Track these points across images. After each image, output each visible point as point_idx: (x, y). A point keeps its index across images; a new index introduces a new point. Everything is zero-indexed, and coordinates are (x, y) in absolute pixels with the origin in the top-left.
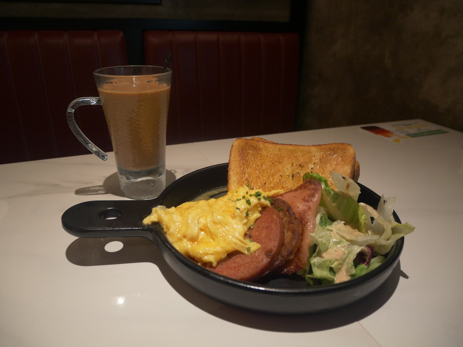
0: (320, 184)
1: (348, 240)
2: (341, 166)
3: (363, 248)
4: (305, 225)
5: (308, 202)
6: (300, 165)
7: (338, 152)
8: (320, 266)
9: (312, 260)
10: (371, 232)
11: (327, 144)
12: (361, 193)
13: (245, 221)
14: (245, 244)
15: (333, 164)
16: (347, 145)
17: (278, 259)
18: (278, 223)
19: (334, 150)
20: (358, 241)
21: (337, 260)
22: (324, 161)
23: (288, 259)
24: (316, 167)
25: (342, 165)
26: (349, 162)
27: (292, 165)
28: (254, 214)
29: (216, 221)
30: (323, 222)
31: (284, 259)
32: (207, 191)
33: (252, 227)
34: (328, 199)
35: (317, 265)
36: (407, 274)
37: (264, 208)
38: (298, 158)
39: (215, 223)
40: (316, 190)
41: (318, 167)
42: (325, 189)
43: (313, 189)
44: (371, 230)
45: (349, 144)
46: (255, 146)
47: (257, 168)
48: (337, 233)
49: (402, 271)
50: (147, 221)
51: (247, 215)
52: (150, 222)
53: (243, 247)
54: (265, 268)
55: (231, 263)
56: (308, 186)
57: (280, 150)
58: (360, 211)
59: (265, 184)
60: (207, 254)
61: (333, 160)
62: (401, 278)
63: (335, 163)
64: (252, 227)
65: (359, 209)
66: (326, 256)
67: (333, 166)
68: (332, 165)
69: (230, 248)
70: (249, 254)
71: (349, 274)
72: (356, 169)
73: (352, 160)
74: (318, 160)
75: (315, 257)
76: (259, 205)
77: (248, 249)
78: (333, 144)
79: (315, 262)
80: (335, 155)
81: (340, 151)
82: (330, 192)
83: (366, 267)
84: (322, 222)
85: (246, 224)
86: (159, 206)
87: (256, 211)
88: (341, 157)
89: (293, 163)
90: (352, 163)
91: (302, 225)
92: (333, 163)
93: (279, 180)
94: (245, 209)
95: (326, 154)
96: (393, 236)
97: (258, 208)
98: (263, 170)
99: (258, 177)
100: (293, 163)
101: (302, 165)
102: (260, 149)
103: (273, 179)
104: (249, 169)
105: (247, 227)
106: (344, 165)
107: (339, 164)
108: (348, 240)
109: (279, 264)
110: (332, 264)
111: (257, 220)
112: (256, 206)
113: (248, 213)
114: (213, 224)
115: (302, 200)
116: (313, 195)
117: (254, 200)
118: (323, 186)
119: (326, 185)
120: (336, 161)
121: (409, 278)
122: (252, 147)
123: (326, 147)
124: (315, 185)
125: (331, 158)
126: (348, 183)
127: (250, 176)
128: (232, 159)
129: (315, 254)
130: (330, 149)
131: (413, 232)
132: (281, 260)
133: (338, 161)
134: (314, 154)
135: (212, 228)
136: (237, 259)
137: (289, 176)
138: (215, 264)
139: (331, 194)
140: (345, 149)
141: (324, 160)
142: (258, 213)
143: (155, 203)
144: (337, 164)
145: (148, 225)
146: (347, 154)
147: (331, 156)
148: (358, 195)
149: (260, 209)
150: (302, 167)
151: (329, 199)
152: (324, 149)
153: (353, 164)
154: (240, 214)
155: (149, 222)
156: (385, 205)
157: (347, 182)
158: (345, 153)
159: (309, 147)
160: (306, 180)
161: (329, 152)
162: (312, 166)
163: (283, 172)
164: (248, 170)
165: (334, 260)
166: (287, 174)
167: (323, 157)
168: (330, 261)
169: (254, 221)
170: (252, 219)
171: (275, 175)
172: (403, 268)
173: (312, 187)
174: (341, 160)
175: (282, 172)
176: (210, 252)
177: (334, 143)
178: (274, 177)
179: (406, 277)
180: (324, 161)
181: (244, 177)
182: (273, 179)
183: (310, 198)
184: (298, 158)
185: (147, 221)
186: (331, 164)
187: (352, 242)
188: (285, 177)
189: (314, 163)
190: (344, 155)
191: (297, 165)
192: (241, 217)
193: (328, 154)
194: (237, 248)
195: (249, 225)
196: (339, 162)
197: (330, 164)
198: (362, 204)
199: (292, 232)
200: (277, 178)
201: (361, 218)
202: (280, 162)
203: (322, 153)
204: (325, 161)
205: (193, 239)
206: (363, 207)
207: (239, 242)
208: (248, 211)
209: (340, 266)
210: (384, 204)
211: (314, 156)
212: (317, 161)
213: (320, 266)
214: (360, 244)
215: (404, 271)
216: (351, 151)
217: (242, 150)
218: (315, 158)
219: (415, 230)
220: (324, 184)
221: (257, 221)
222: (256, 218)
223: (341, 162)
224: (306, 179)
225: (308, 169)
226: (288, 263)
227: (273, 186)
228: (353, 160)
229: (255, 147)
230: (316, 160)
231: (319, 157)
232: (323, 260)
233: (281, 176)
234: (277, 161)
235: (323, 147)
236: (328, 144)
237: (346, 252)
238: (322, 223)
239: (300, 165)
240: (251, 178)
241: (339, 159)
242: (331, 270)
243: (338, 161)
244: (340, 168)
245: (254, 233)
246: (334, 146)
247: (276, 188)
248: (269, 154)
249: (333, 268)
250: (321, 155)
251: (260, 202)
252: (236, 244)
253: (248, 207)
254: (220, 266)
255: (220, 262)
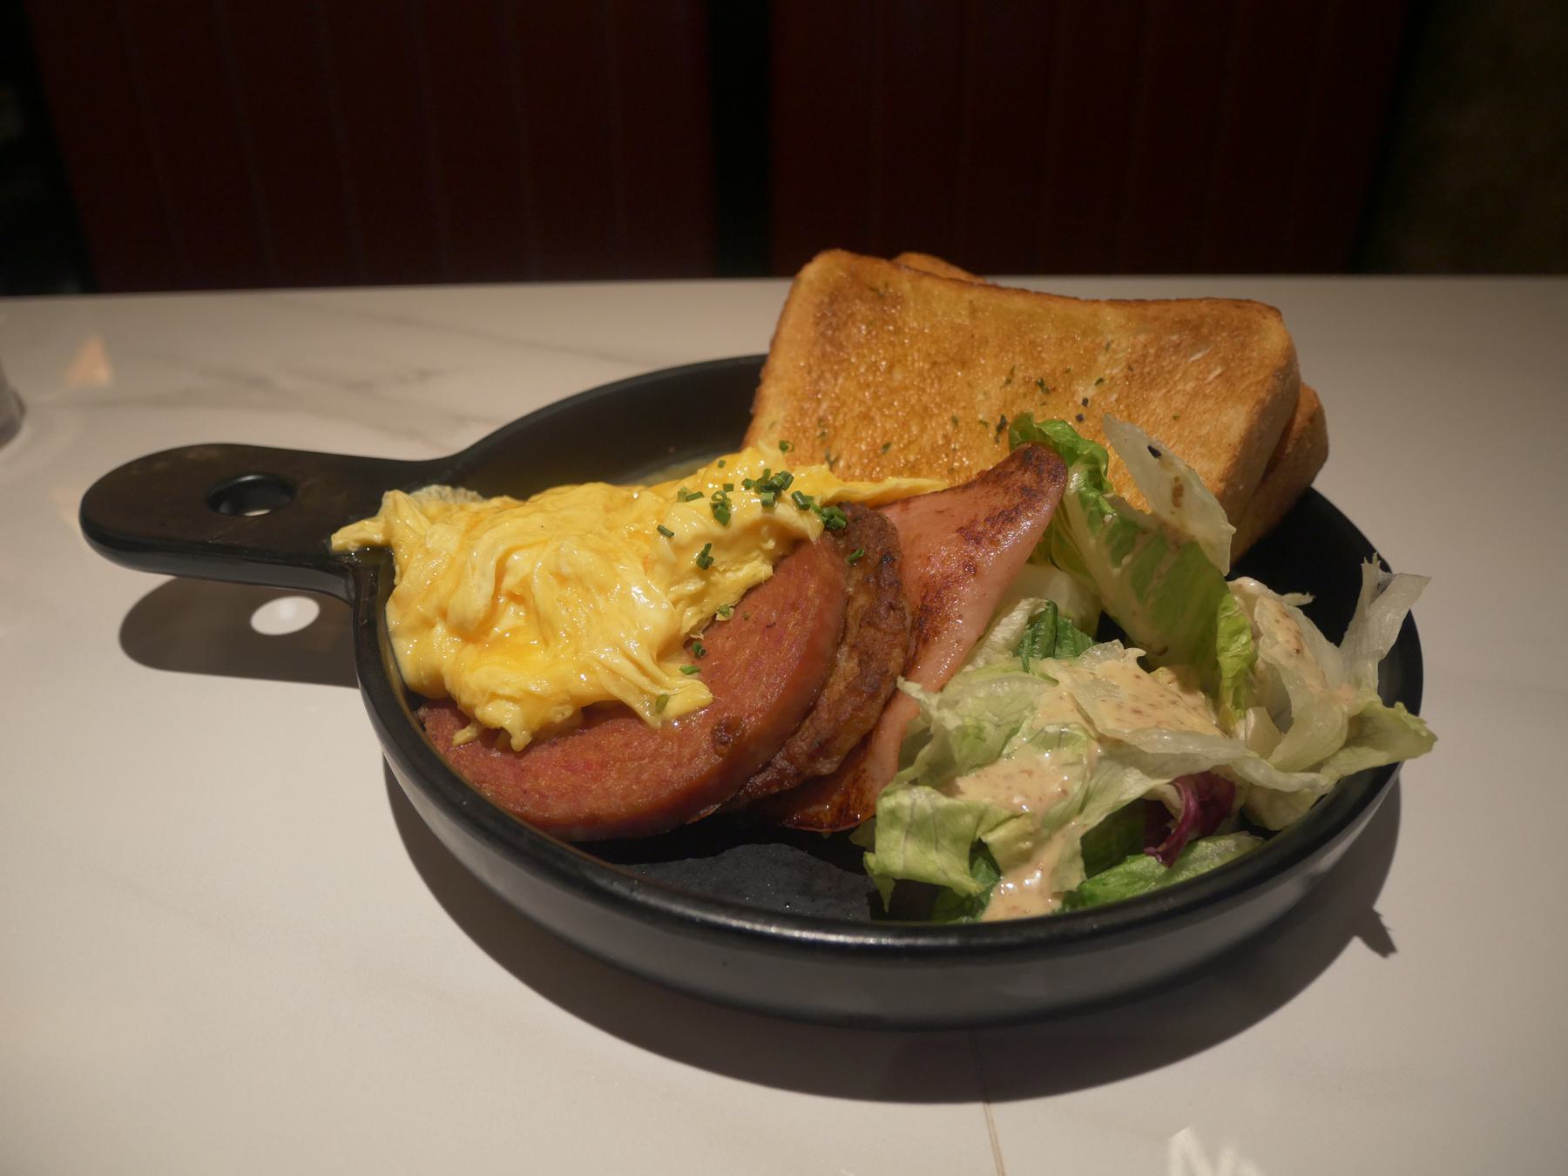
0: (1060, 474)
1: (1101, 739)
2: (1210, 403)
3: (1161, 784)
4: (926, 641)
5: (978, 542)
6: (1041, 384)
7: (1212, 338)
8: (922, 828)
9: (886, 794)
10: (1256, 714)
11: (1173, 297)
12: (1237, 531)
13: (693, 586)
14: (656, 681)
15: (1179, 391)
16: (1259, 312)
17: (768, 764)
18: (813, 612)
19: (1197, 328)
20: (1143, 752)
21: (1015, 816)
22: (1142, 374)
23: (808, 772)
24: (1106, 398)
25: (1217, 399)
26: (1248, 387)
27: (1009, 381)
28: (745, 562)
29: (566, 570)
30: (1037, 639)
31: (791, 770)
32: (672, 450)
33: (719, 617)
34: (1091, 543)
35: (908, 820)
36: (1396, 936)
37: (792, 544)
38: (1041, 352)
39: (563, 580)
40: (1030, 497)
41: (1115, 396)
42: (1080, 494)
43: (1025, 490)
44: (1263, 710)
45: (1272, 309)
46: (880, 284)
47: (871, 378)
48: (1072, 696)
49: (1376, 917)
50: (346, 538)
51: (705, 564)
52: (355, 541)
53: (643, 692)
54: (695, 794)
55: (583, 747)
56: (1013, 472)
57: (973, 311)
58: (1228, 617)
59: (887, 446)
60: (494, 696)
61: (1185, 373)
62: (1356, 947)
63: (1190, 386)
64: (719, 617)
65: (1223, 605)
66: (974, 790)
67: (1178, 402)
68: (1175, 394)
69: (586, 685)
70: (659, 724)
71: (1056, 889)
72: (1296, 427)
73: (1265, 380)
74: (1122, 366)
75: (914, 783)
76: (765, 529)
77: (660, 703)
78: (1200, 300)
79: (900, 807)
80: (1199, 351)
81: (1225, 334)
82: (1103, 514)
83: (1163, 869)
84: (1034, 636)
85: (695, 599)
86: (434, 489)
87: (754, 554)
88: (1225, 362)
89: (1012, 372)
90: (1262, 395)
91: (918, 638)
92: (1179, 388)
93: (945, 436)
94: (697, 538)
95: (1162, 343)
96: (1344, 757)
97: (766, 541)
98: (893, 391)
99: (866, 417)
100: (1012, 372)
101: (1049, 384)
102: (898, 300)
103: (923, 430)
104: (840, 381)
105: (702, 612)
106: (1224, 399)
107: (1204, 395)
108: (1101, 739)
109: (768, 785)
110: (992, 830)
111: (752, 590)
112: (753, 530)
113: (710, 554)
114: (554, 582)
115: (960, 530)
116: (1008, 517)
117: (746, 506)
118: (1076, 479)
119: (1096, 479)
120: (1197, 379)
121: (1393, 957)
122: (872, 289)
123: (1168, 310)
124: (1039, 474)
125: (1178, 365)
126: (1177, 479)
127: (835, 411)
128: (786, 333)
129: (909, 772)
130: (1183, 324)
131: (1424, 757)
132: (782, 771)
133: (1204, 379)
134: (1110, 337)
135: (544, 593)
136: (610, 737)
137: (985, 424)
138: (520, 739)
139: (1104, 522)
140: (1249, 327)
141: (1143, 368)
142: (764, 562)
143: (411, 476)
144: (1195, 395)
145: (345, 553)
146: (1253, 351)
147: (1182, 353)
148: (1228, 539)
149: (771, 544)
150: (1047, 392)
151: (1092, 542)
152: (1156, 319)
153: (1268, 398)
154: (671, 555)
155: (352, 543)
156: (1373, 605)
157: (1172, 475)
158: (1244, 346)
159: (1095, 305)
160: (1022, 446)
161: (1175, 338)
162: (1091, 392)
163: (964, 408)
164: (836, 384)
165: (1005, 813)
166: (980, 417)
167: (1145, 356)
168: (981, 817)
169: (743, 591)
170: (727, 582)
171: (931, 416)
172: (1388, 906)
173: (1023, 482)
174: (1220, 375)
175: (963, 404)
176: (507, 691)
177: (1207, 299)
178: (926, 422)
179: (1382, 943)
180: (1142, 374)
181: (815, 411)
182: (923, 430)
183: (992, 526)
184: (1041, 352)
185: (346, 538)
186: (1168, 392)
187: (1119, 752)
188: (970, 430)
189: (1100, 381)
190: (1240, 354)
191: (1026, 382)
192: (673, 568)
193: (1167, 347)
194: (616, 691)
195: (708, 606)
196: (1209, 384)
197: (1168, 388)
198: (1250, 584)
199: (860, 663)
200: (939, 427)
201: (1225, 650)
202: (964, 364)
203: (1142, 338)
204: (1149, 373)
205: (473, 632)
206: (1250, 600)
207: (629, 670)
208: (708, 547)
209: (1028, 844)
210: (1372, 602)
211: (1107, 350)
212: (1115, 371)
213: (922, 828)
214: (1149, 766)
215: (1386, 921)
216: (1272, 339)
217: (833, 300)
218: (1111, 357)
219: (1436, 745)
220: (1086, 473)
221: (753, 596)
222: (751, 582)
223: (1217, 387)
224: (1018, 445)
225: (1067, 403)
226: (815, 787)
227: (917, 459)
228: (1267, 385)
229: (881, 291)
230: (1112, 369)
231: (1128, 356)
232: (943, 801)
233: (955, 421)
234: (951, 355)
235: (1152, 311)
236: (1178, 300)
237: (1076, 789)
238: (1034, 643)
239: (1041, 384)
240: (841, 416)
241: (1209, 372)
242: (979, 851)
243: (1206, 382)
244: (1204, 413)
245: (723, 642)
246: (1204, 308)
247: (925, 472)
248: (927, 325)
249: (992, 849)
250: (1139, 348)
251: (769, 515)
252: (614, 674)
253: (716, 529)
254: (541, 753)
255: (545, 735)
